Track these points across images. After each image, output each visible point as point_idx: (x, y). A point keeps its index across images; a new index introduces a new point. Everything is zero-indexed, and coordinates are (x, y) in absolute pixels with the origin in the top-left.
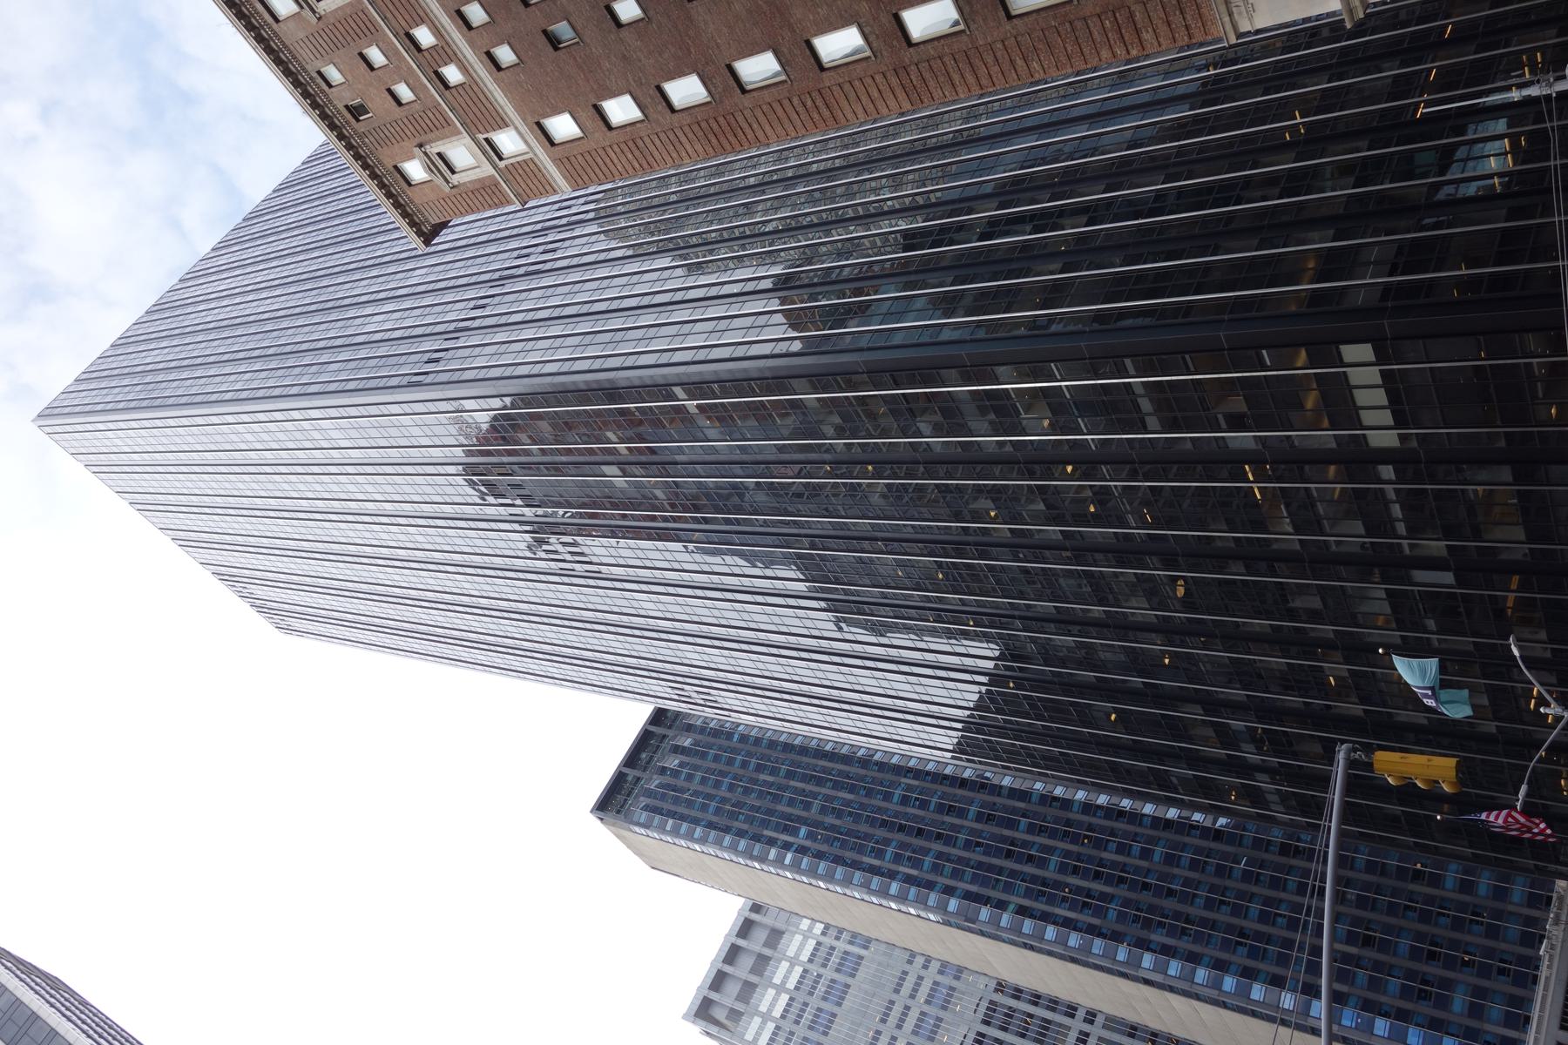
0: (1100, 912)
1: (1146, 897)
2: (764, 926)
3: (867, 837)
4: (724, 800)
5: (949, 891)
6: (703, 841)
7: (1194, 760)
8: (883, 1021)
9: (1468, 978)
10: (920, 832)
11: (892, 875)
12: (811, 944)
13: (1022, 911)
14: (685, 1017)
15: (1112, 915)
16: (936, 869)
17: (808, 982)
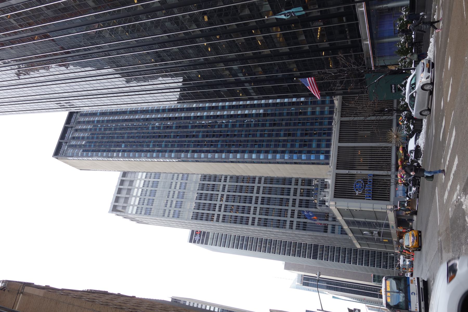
0: (216, 146)
1: (228, 138)
2: (127, 180)
3: (143, 142)
4: (96, 142)
5: (171, 151)
6: (92, 156)
7: (226, 84)
8: (168, 197)
9: (316, 137)
10: (159, 136)
11: (153, 151)
12: (143, 182)
13: (194, 152)
14: (109, 212)
15: (219, 146)
16: (166, 146)
17: (144, 192)
